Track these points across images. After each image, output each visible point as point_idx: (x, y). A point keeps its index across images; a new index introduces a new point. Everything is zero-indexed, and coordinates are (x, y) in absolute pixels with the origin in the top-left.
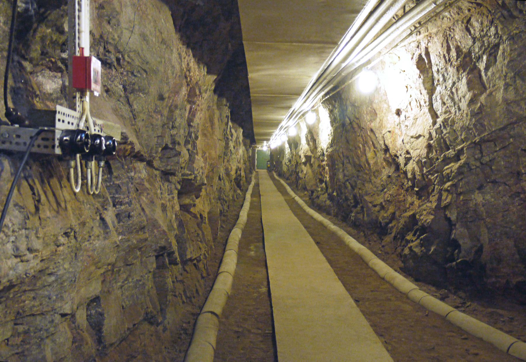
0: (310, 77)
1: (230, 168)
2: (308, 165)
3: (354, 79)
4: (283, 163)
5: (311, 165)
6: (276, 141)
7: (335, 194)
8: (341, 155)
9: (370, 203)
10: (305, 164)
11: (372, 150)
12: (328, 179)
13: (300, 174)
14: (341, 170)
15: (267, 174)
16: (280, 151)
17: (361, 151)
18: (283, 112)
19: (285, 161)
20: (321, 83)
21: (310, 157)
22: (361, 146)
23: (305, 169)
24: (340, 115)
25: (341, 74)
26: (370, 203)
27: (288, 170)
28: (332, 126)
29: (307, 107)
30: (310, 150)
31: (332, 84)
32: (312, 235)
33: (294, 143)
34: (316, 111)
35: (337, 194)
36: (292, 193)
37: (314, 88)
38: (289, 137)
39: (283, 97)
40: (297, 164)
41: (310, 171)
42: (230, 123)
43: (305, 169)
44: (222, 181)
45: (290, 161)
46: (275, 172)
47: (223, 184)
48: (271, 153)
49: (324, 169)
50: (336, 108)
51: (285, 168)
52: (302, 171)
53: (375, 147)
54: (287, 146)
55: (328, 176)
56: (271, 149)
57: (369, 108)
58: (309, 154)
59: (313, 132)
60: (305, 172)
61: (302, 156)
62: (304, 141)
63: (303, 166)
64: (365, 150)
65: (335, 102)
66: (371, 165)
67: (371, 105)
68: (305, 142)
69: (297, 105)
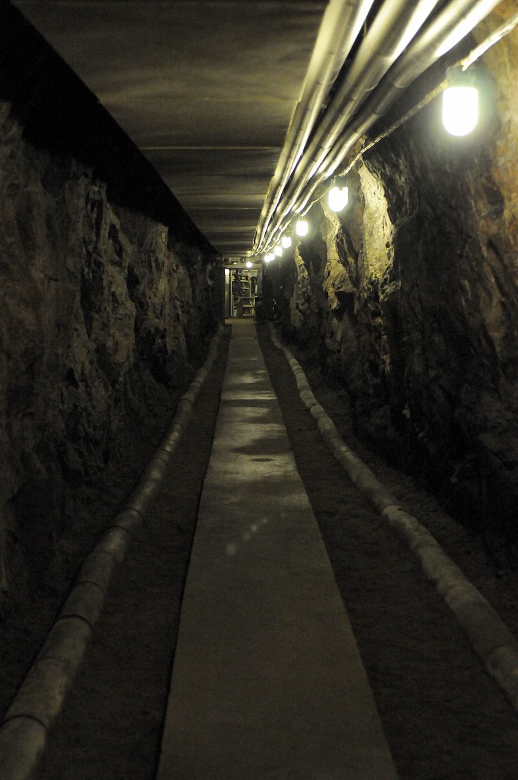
0: (286, 98)
1: (110, 344)
2: (346, 317)
3: (429, 98)
4: (292, 304)
5: (354, 320)
6: (276, 244)
7: (407, 412)
8: (418, 308)
9: (496, 454)
10: (338, 313)
11: (495, 301)
12: (388, 368)
13: (328, 341)
14: (418, 350)
15: (255, 332)
16: (286, 269)
17: (467, 300)
18: (252, 186)
19: (296, 301)
20: (340, 111)
21: (352, 295)
22: (466, 283)
23: (339, 327)
24: (411, 193)
25: (391, 85)
26: (496, 454)
27: (305, 323)
28: (393, 221)
29: (324, 166)
30: (351, 278)
31: (374, 111)
32: (331, 547)
33: (313, 253)
34: (354, 180)
35: (412, 413)
36: (307, 396)
37: (325, 123)
38: (284, 249)
39: (252, 148)
40: (321, 313)
41: (351, 333)
42: (110, 217)
43: (339, 327)
44: (82, 386)
45: (308, 300)
46: (276, 326)
47: (83, 395)
48: (264, 277)
49: (380, 337)
50: (400, 173)
51: (296, 319)
52: (333, 334)
53: (503, 294)
54: (299, 260)
55: (387, 358)
56: (264, 266)
57: (484, 180)
58: (348, 288)
59: (351, 233)
60: (339, 337)
61: (331, 291)
62: (333, 254)
63: (335, 321)
64: (477, 297)
65: (398, 156)
66: (496, 344)
67: (488, 171)
68: (336, 256)
69: (288, 164)
